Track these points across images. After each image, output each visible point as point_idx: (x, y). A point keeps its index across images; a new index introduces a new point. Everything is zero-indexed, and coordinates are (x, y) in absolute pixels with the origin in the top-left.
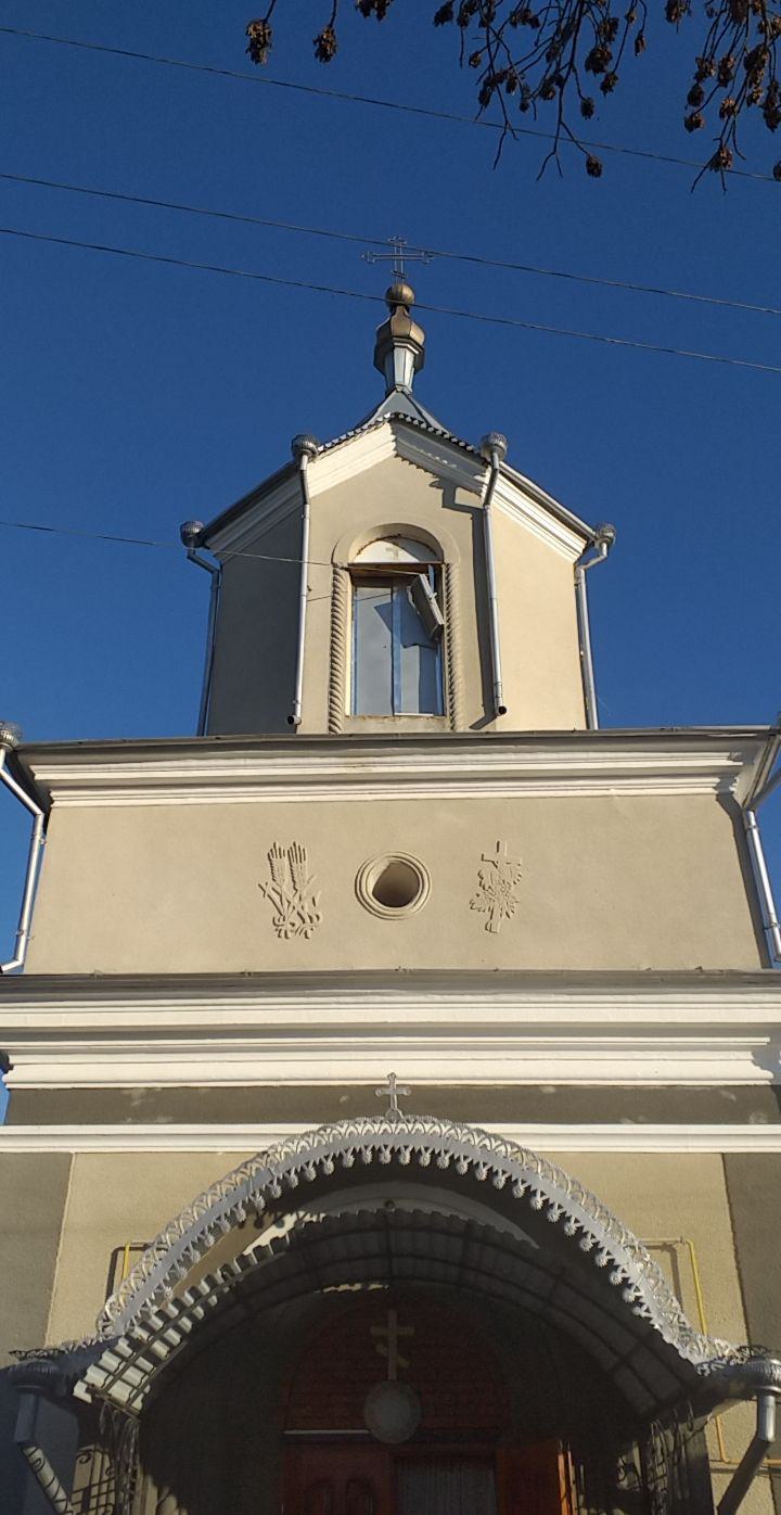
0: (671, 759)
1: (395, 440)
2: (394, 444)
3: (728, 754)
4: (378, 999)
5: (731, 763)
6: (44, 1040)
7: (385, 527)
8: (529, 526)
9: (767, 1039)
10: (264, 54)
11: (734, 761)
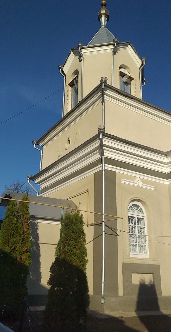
1: (74, 54)
2: (74, 54)
3: (100, 92)
5: (101, 93)
7: (74, 73)
9: (99, 150)
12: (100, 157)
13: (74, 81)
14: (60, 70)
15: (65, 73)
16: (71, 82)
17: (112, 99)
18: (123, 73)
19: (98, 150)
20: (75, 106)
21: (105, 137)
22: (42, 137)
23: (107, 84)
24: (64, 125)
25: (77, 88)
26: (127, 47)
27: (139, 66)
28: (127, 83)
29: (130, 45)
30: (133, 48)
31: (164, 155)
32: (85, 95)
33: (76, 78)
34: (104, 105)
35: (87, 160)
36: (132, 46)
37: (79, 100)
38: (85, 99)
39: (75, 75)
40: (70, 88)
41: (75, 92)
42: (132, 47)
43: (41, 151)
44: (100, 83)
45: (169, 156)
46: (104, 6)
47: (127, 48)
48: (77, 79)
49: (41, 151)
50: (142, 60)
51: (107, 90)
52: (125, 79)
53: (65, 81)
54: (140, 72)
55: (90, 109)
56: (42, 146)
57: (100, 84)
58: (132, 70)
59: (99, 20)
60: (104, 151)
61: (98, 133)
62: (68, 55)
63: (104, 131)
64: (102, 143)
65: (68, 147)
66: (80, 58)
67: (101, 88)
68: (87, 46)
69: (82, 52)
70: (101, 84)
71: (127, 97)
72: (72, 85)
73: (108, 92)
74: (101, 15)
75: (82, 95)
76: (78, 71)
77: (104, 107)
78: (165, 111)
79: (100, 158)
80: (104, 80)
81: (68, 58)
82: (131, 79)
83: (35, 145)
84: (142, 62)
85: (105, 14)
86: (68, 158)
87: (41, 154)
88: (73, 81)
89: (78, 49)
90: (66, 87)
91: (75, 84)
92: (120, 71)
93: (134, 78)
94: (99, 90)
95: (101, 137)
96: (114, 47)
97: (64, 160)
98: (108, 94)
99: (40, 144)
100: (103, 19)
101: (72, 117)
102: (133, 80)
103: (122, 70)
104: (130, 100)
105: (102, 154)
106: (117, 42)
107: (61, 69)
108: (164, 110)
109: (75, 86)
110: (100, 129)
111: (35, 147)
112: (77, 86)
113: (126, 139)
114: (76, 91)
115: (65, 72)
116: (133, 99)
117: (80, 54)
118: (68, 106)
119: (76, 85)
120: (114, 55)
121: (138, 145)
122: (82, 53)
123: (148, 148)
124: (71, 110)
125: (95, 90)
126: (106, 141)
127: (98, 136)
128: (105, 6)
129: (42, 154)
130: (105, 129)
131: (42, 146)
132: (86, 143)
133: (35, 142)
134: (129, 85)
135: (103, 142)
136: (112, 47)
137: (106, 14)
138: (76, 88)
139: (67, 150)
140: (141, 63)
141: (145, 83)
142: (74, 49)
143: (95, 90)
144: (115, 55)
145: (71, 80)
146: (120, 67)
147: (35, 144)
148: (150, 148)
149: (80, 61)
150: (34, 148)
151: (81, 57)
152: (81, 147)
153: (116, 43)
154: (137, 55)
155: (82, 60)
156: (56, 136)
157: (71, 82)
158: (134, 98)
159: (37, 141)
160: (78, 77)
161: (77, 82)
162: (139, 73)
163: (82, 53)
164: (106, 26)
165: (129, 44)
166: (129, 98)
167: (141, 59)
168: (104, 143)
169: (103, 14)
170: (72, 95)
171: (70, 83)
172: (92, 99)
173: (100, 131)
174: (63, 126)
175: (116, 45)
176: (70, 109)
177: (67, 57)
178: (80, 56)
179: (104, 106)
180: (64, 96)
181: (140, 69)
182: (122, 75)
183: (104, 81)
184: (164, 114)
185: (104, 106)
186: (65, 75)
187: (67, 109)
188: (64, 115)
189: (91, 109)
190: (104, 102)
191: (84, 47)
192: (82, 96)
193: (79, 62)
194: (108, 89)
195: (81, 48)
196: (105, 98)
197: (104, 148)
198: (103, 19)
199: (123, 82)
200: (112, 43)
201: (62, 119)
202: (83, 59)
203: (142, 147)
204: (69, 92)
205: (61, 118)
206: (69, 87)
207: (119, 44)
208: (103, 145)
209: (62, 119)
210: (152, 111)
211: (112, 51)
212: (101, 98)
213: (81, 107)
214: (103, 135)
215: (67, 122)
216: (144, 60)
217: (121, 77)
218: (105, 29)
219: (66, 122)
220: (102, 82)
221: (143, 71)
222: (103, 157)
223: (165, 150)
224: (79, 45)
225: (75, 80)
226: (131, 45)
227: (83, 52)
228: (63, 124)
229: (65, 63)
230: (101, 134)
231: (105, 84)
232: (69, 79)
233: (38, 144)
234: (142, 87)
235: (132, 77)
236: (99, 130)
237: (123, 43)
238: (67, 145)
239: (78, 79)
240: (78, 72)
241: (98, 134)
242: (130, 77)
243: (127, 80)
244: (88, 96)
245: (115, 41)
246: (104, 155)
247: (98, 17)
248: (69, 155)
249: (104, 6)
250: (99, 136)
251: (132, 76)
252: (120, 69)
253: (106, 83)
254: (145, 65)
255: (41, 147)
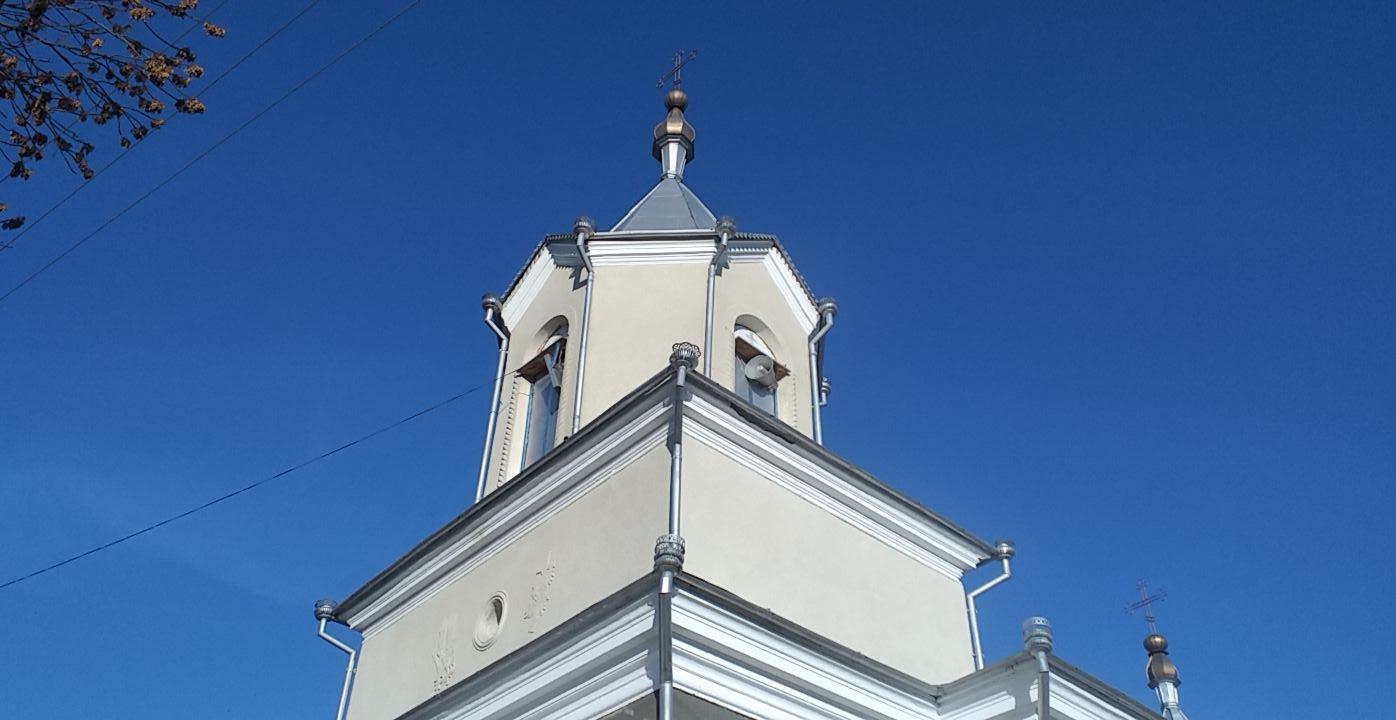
0: (616, 439)
1: (553, 257)
2: (552, 260)
3: (661, 403)
4: (483, 699)
5: (667, 408)
6: (714, 604)
7: (545, 327)
8: (634, 262)
9: (646, 652)
10: (198, 114)
11: (668, 405)
12: (647, 689)
13: (547, 357)
14: (490, 312)
15: (506, 328)
16: (533, 360)
17: (712, 435)
18: (745, 347)
19: (642, 654)
20: (540, 457)
21: (680, 591)
22: (368, 585)
23: (694, 371)
24: (480, 533)
25: (557, 384)
26: (767, 253)
27: (809, 328)
28: (759, 386)
29: (775, 249)
30: (786, 262)
31: (929, 701)
32: (590, 412)
33: (554, 345)
34: (677, 454)
35: (586, 699)
36: (785, 253)
37: (563, 431)
38: (596, 428)
39: (549, 338)
40: (525, 386)
41: (544, 404)
42: (783, 256)
43: (349, 653)
44: (667, 364)
45: (948, 706)
46: (676, 111)
47: (767, 257)
48: (559, 351)
49: (349, 653)
50: (821, 308)
51: (695, 398)
52: (753, 370)
53: (506, 355)
54: (813, 351)
55: (613, 469)
56: (360, 630)
57: (669, 368)
58: (780, 339)
59: (658, 153)
60: (676, 659)
61: (651, 569)
62: (528, 261)
63: (682, 560)
64: (670, 618)
65: (489, 635)
66: (576, 275)
67: (671, 384)
68: (612, 232)
69: (588, 254)
70: (672, 371)
71: (774, 436)
72: (534, 372)
73: (696, 404)
74: (667, 137)
75: (578, 414)
76: (567, 321)
77: (677, 461)
78: (922, 509)
79: (651, 690)
80: (684, 353)
81: (526, 269)
82: (780, 372)
83: (324, 621)
84: (820, 314)
85: (681, 137)
86: (490, 688)
87: (350, 669)
88: (543, 354)
89: (576, 241)
90: (506, 378)
91: (549, 368)
92: (736, 336)
93: (788, 367)
94: (660, 392)
95: (665, 588)
96: (717, 247)
97: (467, 698)
98: (695, 412)
99: (348, 622)
100: (673, 151)
101: (526, 501)
102: (786, 378)
103: (743, 334)
104: (784, 449)
105: (665, 669)
106: (731, 231)
107: (493, 308)
108: (919, 504)
109: (549, 378)
110: (662, 552)
111: (325, 631)
112: (556, 379)
113: (772, 610)
114: (552, 398)
115: (509, 324)
116: (794, 446)
117: (583, 258)
118: (509, 455)
119: (552, 371)
120: (717, 277)
121: (820, 643)
122: (589, 257)
123: (861, 661)
124: (518, 472)
125: (642, 391)
126: (686, 614)
127: (653, 581)
128: (682, 108)
129: (355, 666)
130: (683, 552)
131: (360, 630)
132: (591, 615)
133: (326, 608)
134: (770, 393)
135: (673, 612)
136: (710, 246)
137: (686, 139)
138: (551, 384)
139: (482, 648)
140: (814, 318)
141: (827, 395)
142: (557, 241)
143: (642, 391)
144: (720, 275)
145: (530, 355)
146: (736, 324)
147: (329, 620)
148: (872, 661)
149: (578, 284)
150: (319, 636)
151: (584, 270)
152: (560, 633)
153: (725, 234)
154: (801, 286)
155: (585, 282)
156: (435, 585)
157: (530, 362)
158: (801, 439)
159: (339, 604)
160: (563, 342)
161: (557, 362)
162: (810, 356)
163: (589, 257)
164: (681, 177)
165: (772, 243)
166: (778, 438)
167: (818, 305)
168: (677, 618)
169: (674, 135)
170: (529, 414)
171: (527, 365)
172: (612, 436)
173: (664, 563)
174: (480, 538)
175: (729, 240)
176: (513, 470)
177: (524, 268)
178: (579, 269)
179: (681, 460)
180: (493, 415)
181: (810, 338)
182: (744, 352)
183: (683, 360)
184: (920, 521)
185: (681, 460)
186: (508, 335)
187: (502, 467)
188: (487, 494)
189: (614, 472)
190: (680, 443)
191: (598, 234)
192: (579, 417)
193: (574, 289)
194: (700, 392)
195: (587, 237)
196: (683, 428)
197: (675, 642)
198: (673, 151)
199: (748, 379)
200: (709, 230)
201: (472, 509)
202: (590, 277)
203: (841, 652)
204: (517, 401)
205: (472, 505)
206: (522, 379)
207: (735, 238)
208: (673, 629)
209: (476, 509)
210: (868, 501)
211: (709, 261)
212: (667, 427)
213: (554, 472)
214: (675, 582)
215: (498, 520)
216: (829, 307)
217: (741, 362)
218: (681, 188)
219: (494, 523)
220: (676, 360)
221: (823, 348)
222: (667, 686)
223: (934, 678)
224: (579, 226)
225: (552, 356)
226: (779, 250)
227: (592, 253)
228: (476, 531)
229: (513, 288)
230: (668, 574)
231: (689, 370)
232: (523, 348)
233: (340, 618)
234: (821, 407)
235: (781, 366)
236: (656, 558)
237: (752, 239)
238: (486, 629)
239: (564, 351)
240: (568, 325)
241: (654, 572)
242: (776, 365)
243: (761, 375)
244: (608, 416)
245: (725, 227)
246: (670, 679)
247: (655, 143)
248: (464, 688)
249: (676, 111)
250: (659, 583)
251: (781, 362)
252: (736, 330)
253: (691, 366)
254: (832, 326)
255: (354, 632)
